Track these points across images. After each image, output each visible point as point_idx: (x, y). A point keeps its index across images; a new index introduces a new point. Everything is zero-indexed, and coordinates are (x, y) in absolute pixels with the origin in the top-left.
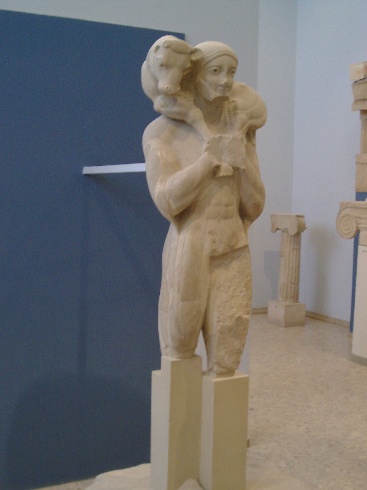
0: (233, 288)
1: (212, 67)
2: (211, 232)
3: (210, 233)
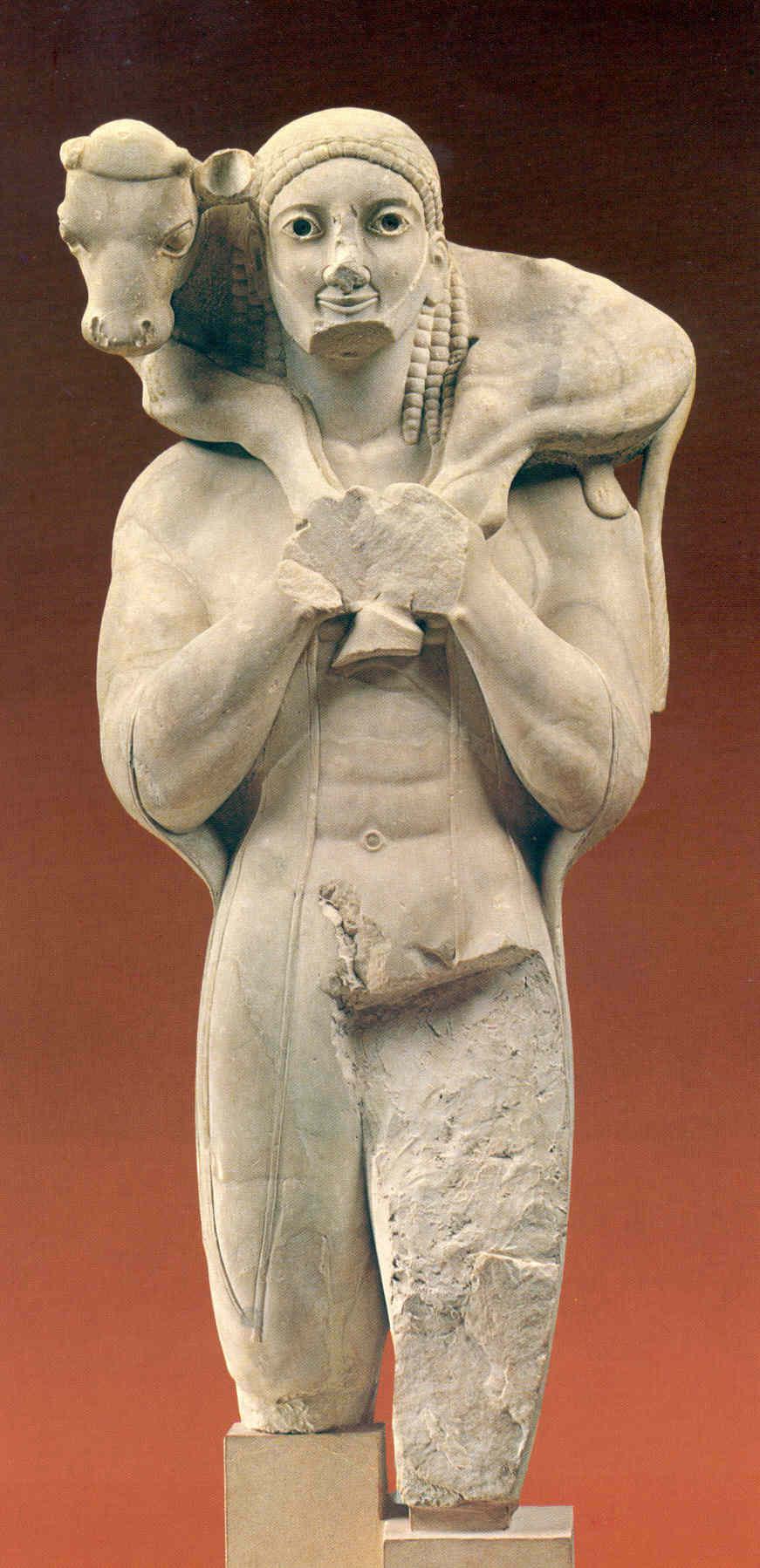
0: (460, 1134)
1: (286, 211)
2: (331, 892)
3: (327, 895)
